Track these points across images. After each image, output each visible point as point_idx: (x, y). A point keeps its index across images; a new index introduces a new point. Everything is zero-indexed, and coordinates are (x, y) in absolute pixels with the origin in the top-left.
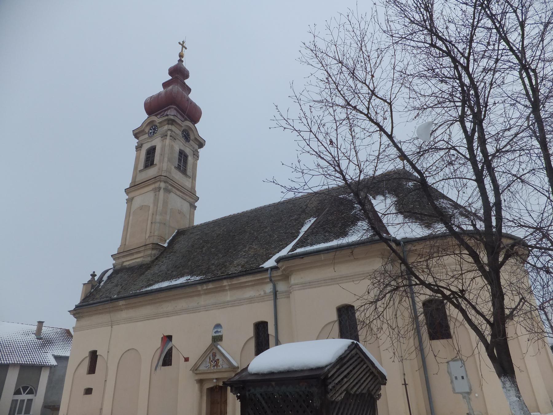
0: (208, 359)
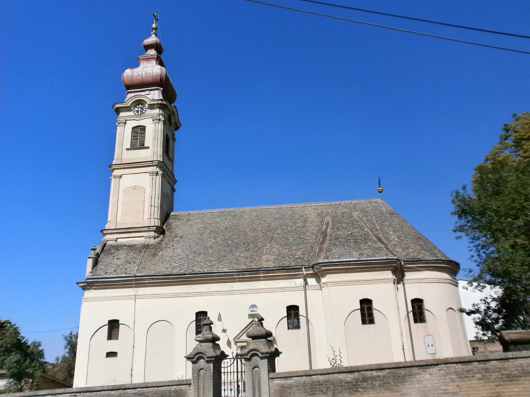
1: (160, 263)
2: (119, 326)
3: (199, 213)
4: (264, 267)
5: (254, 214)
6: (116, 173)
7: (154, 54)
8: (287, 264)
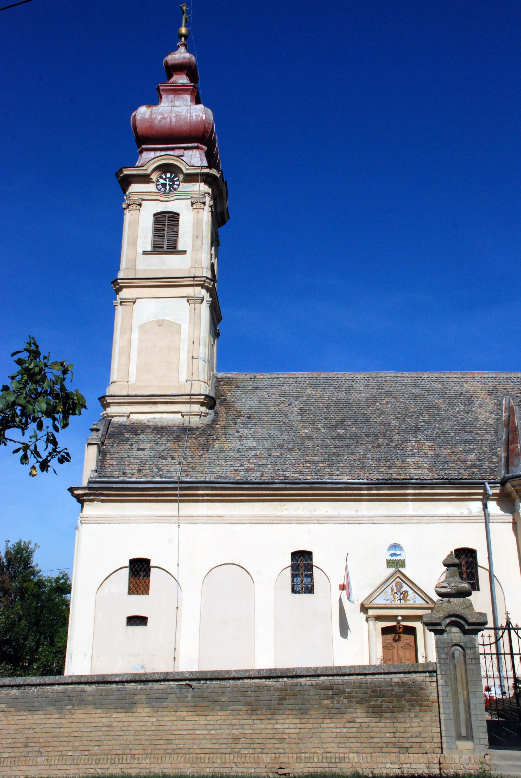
0: (389, 590)
1: (220, 461)
2: (149, 570)
3: (272, 376)
4: (415, 477)
5: (372, 384)
6: (125, 294)
7: (187, 83)
8: (455, 475)
